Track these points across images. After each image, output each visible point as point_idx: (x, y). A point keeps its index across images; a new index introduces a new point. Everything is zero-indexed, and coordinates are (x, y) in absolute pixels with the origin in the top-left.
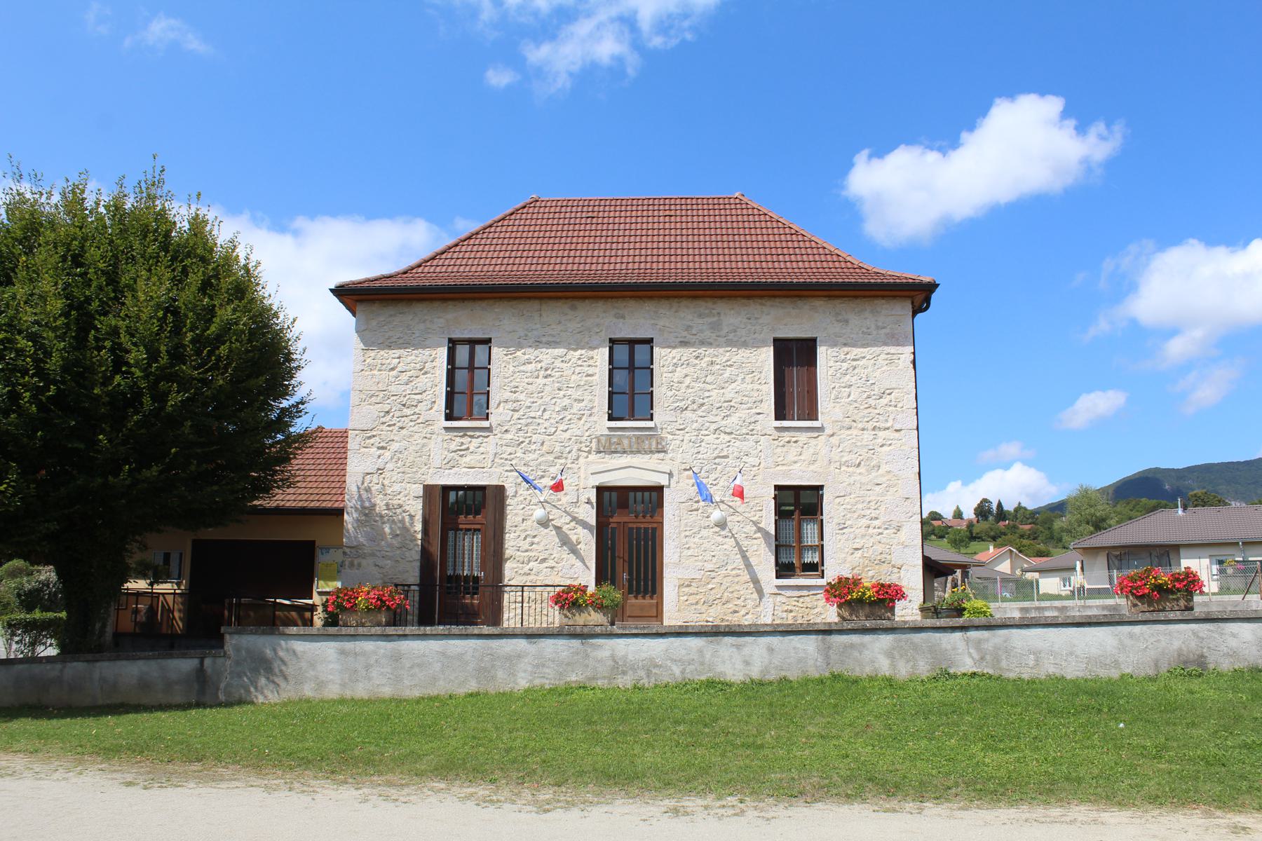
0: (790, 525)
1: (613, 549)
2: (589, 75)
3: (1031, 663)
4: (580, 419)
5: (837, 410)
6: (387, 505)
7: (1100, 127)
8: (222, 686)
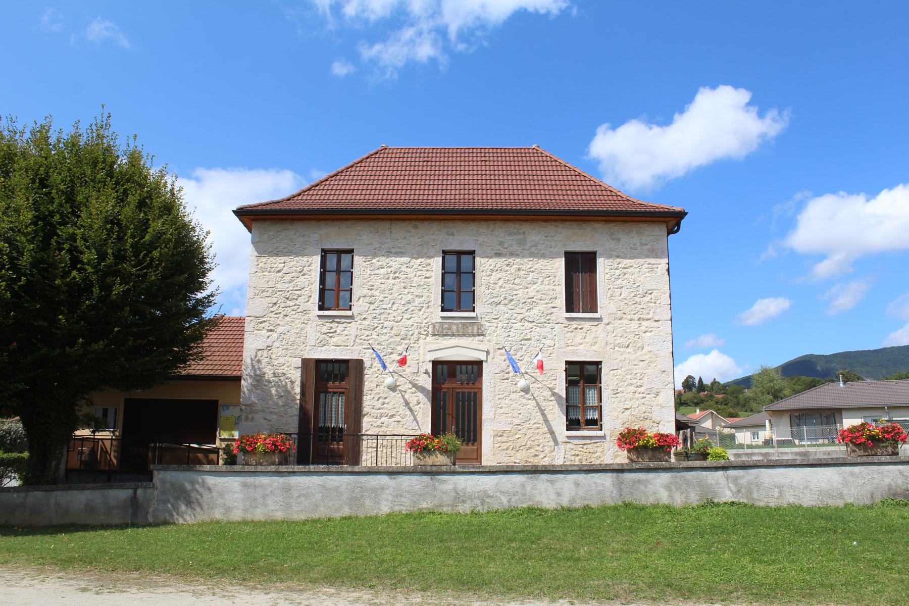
0: (577, 390)
1: (444, 408)
2: (411, 68)
3: (776, 495)
4: (420, 310)
5: (612, 305)
6: (274, 373)
7: (772, 113)
8: (151, 510)
